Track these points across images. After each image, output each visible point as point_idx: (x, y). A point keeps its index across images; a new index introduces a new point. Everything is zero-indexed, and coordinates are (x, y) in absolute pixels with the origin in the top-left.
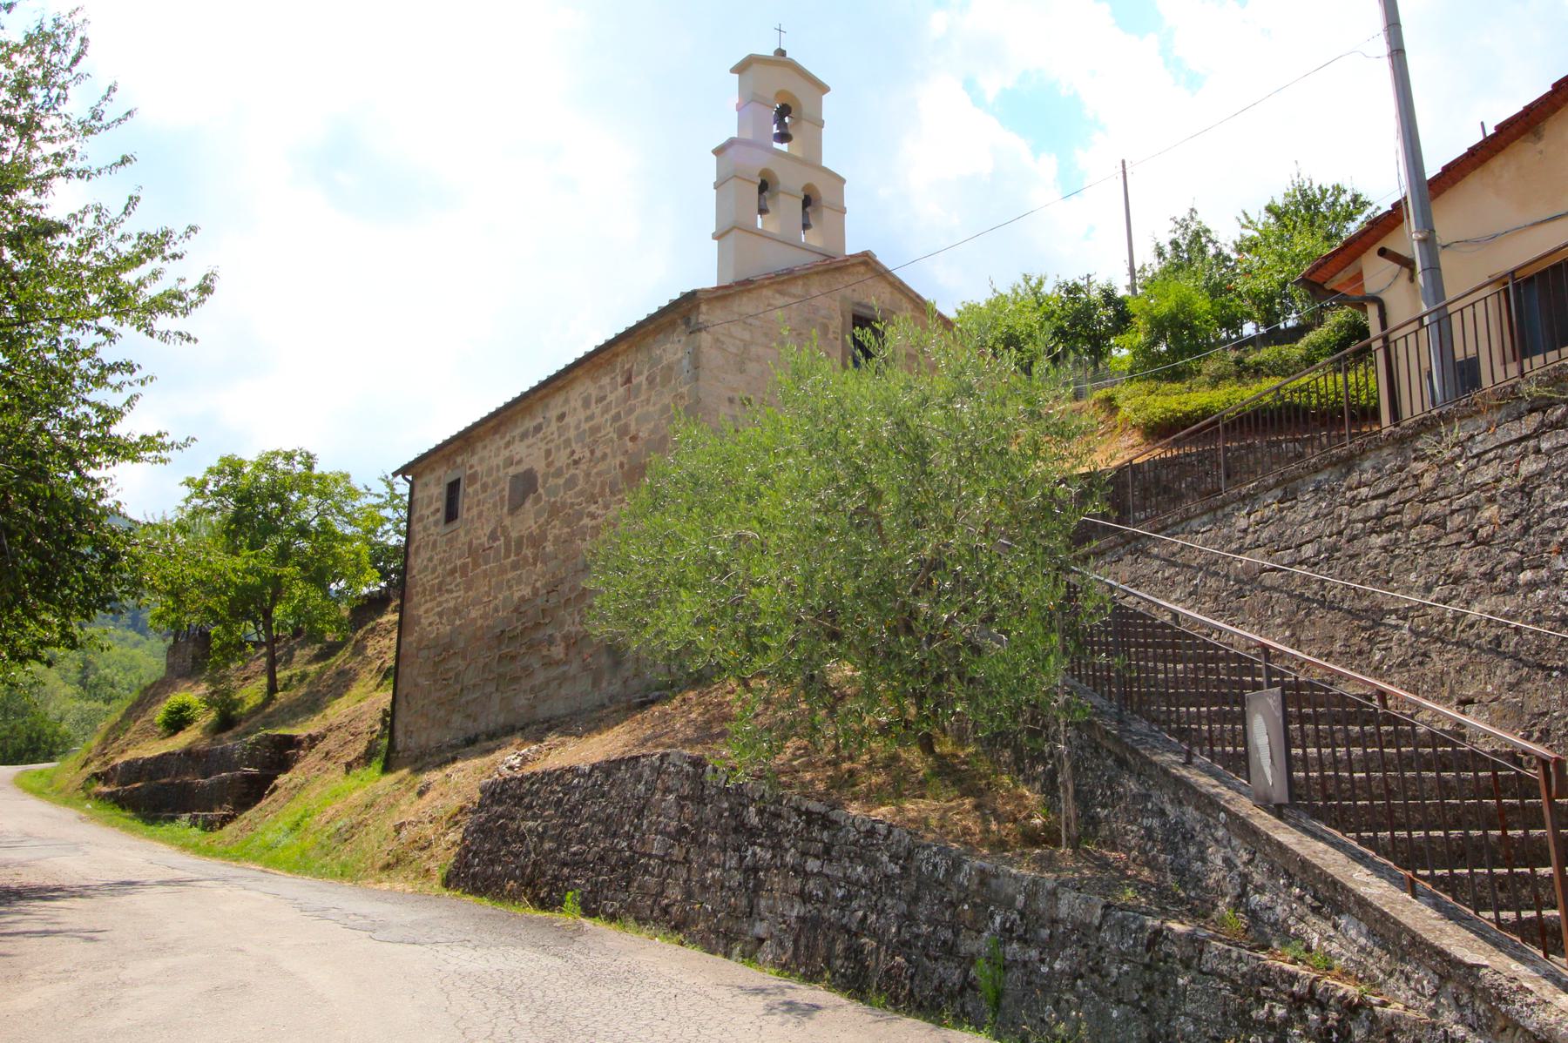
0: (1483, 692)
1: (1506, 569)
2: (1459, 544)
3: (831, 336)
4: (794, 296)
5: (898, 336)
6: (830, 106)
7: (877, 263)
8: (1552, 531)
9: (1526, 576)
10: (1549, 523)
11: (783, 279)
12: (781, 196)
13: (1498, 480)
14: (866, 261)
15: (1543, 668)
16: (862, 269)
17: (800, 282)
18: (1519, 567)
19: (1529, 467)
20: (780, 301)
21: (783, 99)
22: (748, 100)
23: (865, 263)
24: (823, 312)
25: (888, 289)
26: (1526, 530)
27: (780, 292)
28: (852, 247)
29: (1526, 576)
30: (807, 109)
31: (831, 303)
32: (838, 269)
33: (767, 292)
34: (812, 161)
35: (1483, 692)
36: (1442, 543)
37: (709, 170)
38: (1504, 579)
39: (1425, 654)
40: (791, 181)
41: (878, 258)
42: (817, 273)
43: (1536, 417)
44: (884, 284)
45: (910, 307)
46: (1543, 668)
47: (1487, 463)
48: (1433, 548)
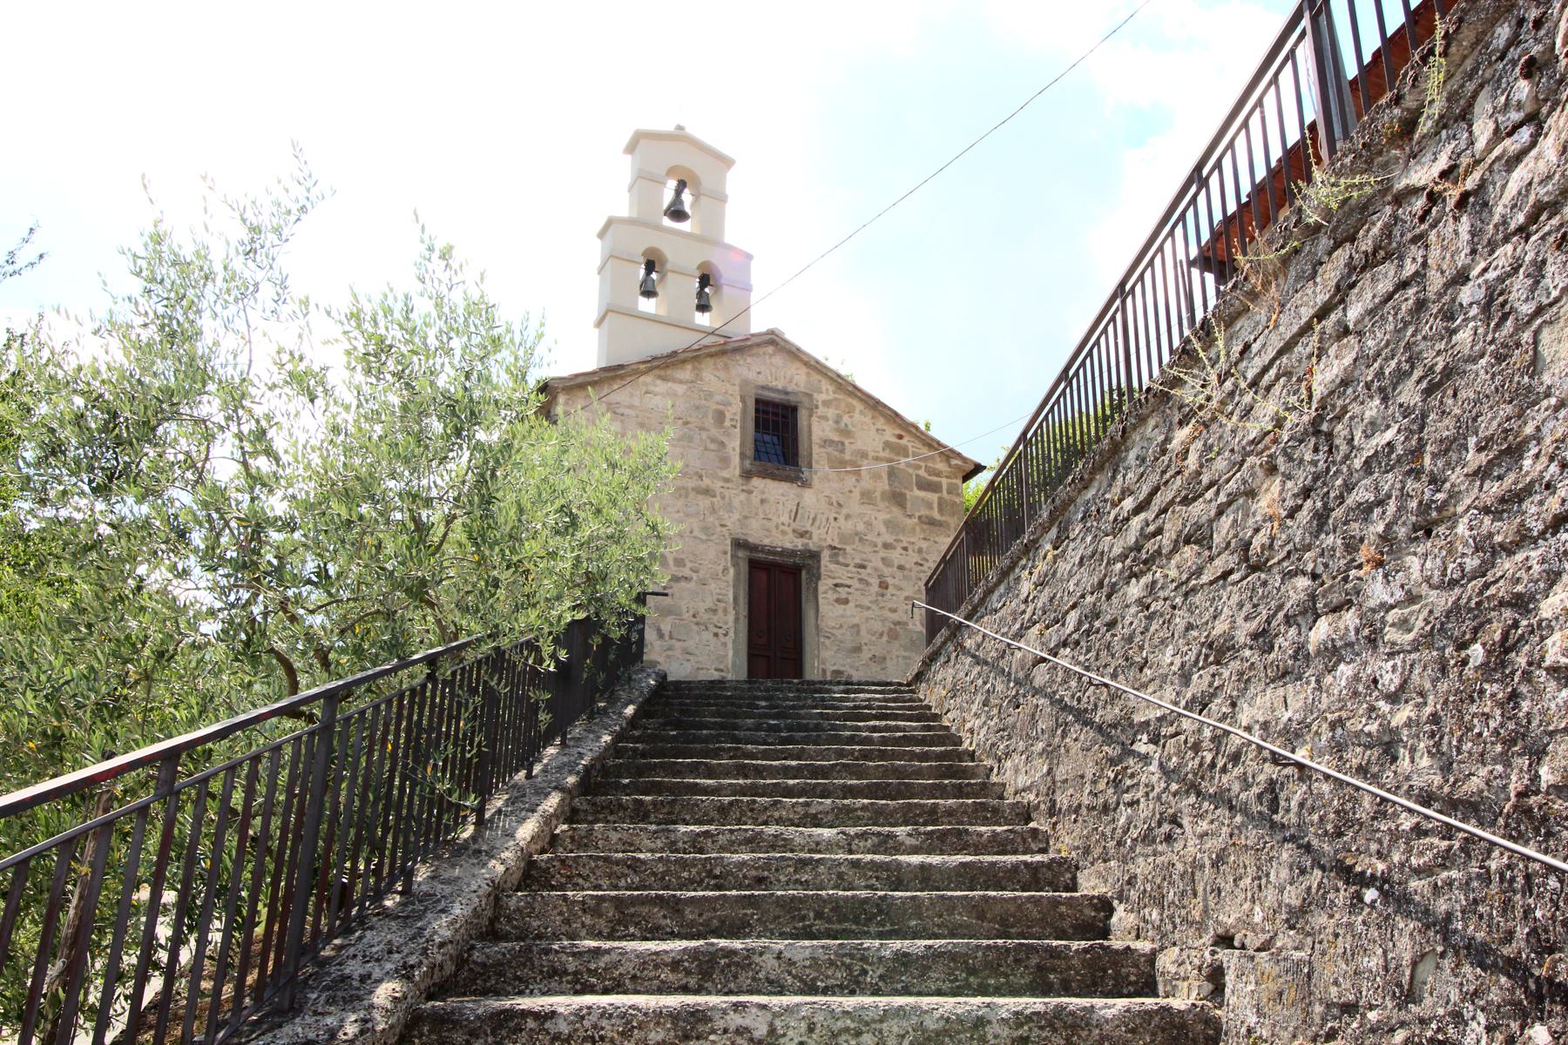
0: (1246, 922)
1: (1288, 620)
2: (1225, 575)
3: (727, 423)
4: (681, 382)
5: (817, 429)
6: (733, 182)
7: (786, 341)
8: (1365, 510)
9: (1321, 631)
10: (1362, 494)
11: (664, 364)
12: (670, 275)
13: (1279, 423)
14: (773, 341)
15: (1346, 873)
16: (770, 349)
17: (689, 367)
18: (1310, 611)
19: (1325, 376)
20: (661, 387)
21: (681, 176)
22: (644, 179)
23: (772, 342)
24: (718, 398)
25: (804, 370)
26: (1321, 518)
27: (664, 379)
28: (758, 324)
29: (1321, 631)
30: (707, 182)
31: (729, 391)
32: (736, 350)
33: (647, 379)
34: (710, 239)
35: (1246, 922)
36: (1205, 579)
37: (595, 251)
38: (1286, 641)
39: (1175, 821)
40: (683, 259)
41: (788, 336)
42: (711, 355)
43: (1342, 255)
44: (798, 364)
45: (831, 388)
46: (1346, 873)
47: (1268, 389)
48: (1194, 590)
